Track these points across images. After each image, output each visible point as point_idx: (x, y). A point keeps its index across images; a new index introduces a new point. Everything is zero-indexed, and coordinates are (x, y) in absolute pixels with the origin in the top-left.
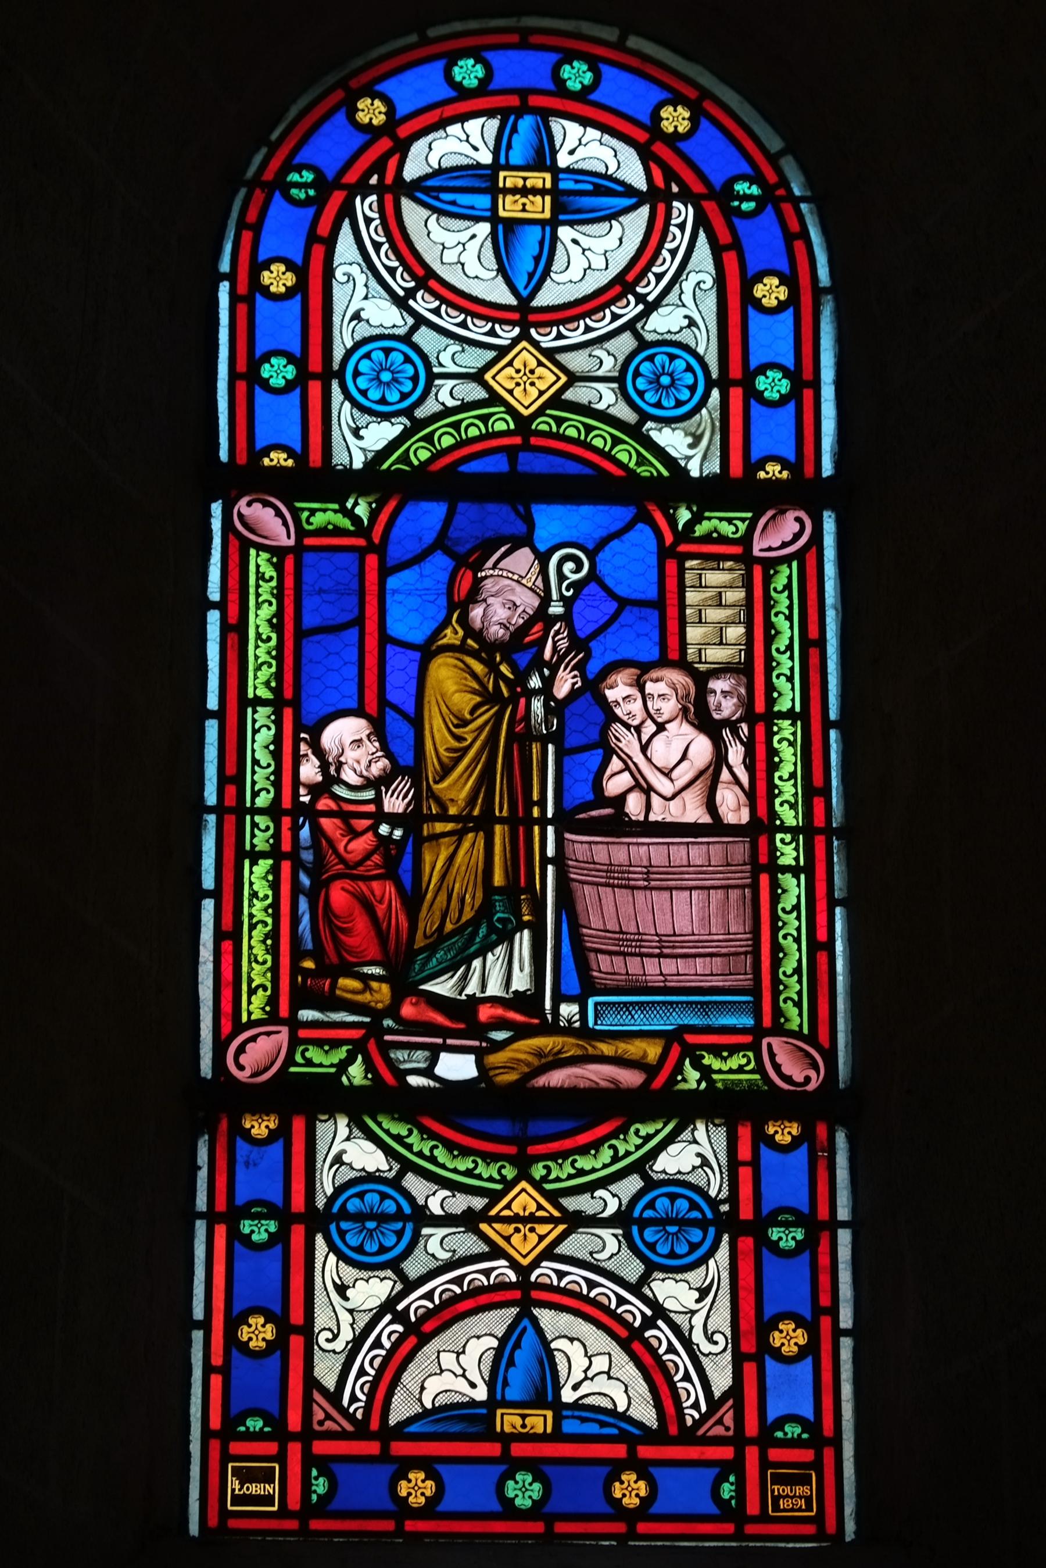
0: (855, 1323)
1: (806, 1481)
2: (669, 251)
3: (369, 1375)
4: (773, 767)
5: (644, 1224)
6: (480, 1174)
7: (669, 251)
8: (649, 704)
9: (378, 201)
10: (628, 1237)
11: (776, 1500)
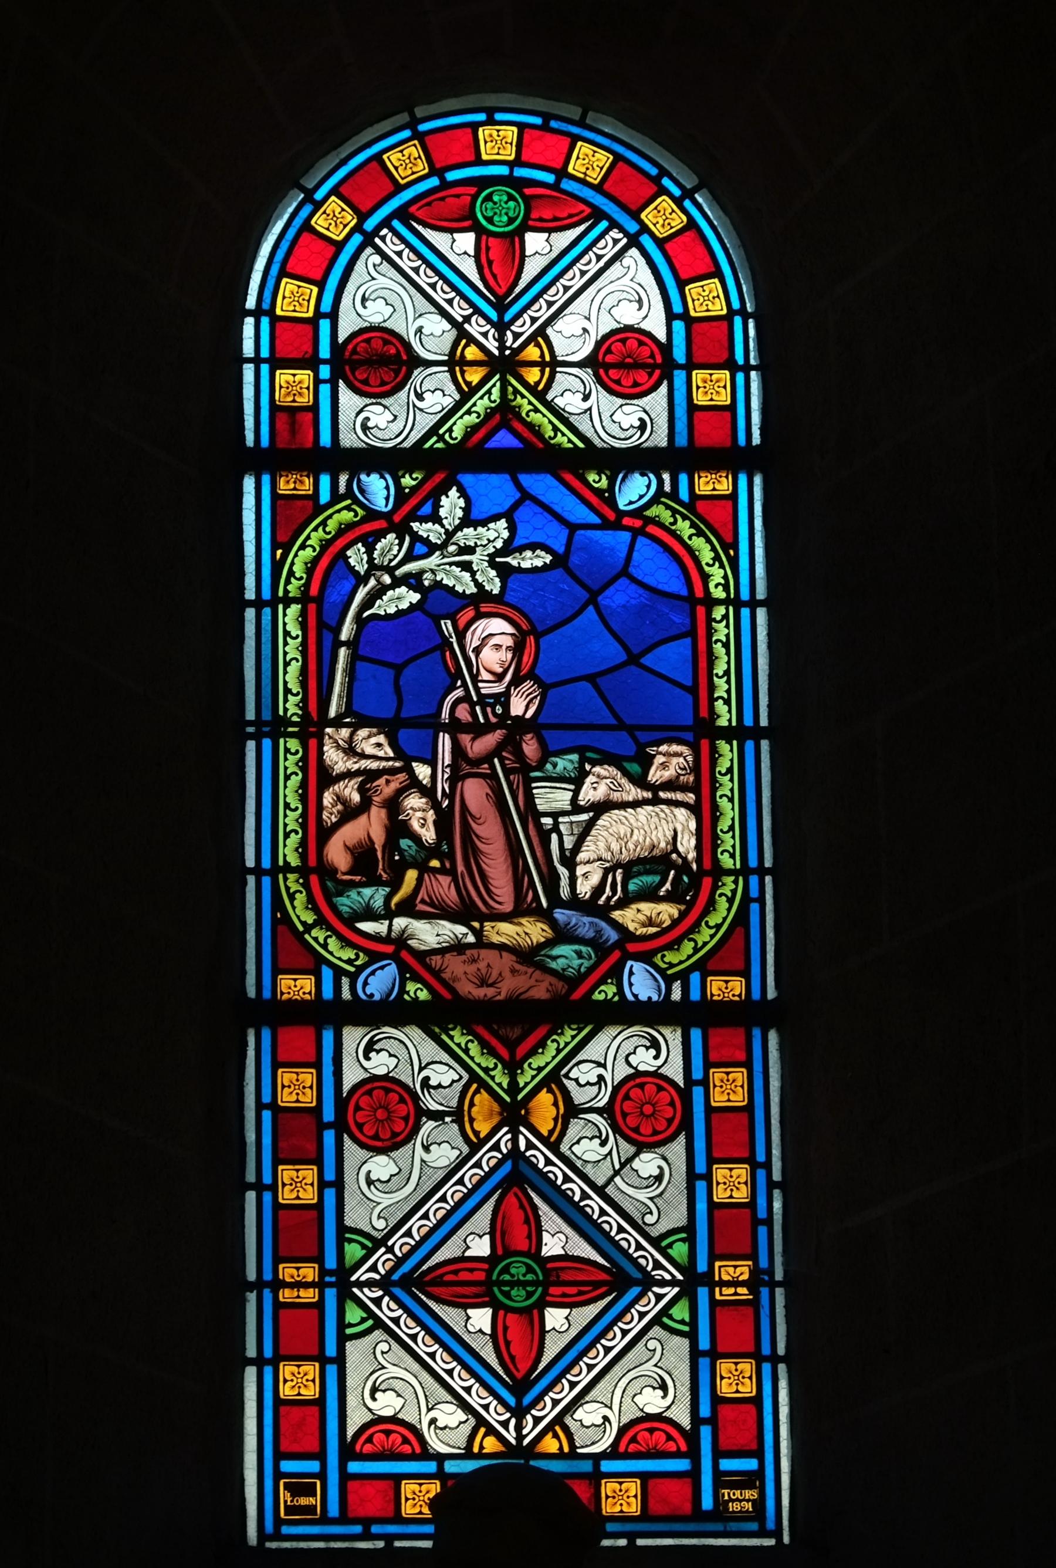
0: (769, 723)
4: (715, 820)
5: (607, 367)
6: (480, 1092)
9: (391, 1299)
10: (596, 375)
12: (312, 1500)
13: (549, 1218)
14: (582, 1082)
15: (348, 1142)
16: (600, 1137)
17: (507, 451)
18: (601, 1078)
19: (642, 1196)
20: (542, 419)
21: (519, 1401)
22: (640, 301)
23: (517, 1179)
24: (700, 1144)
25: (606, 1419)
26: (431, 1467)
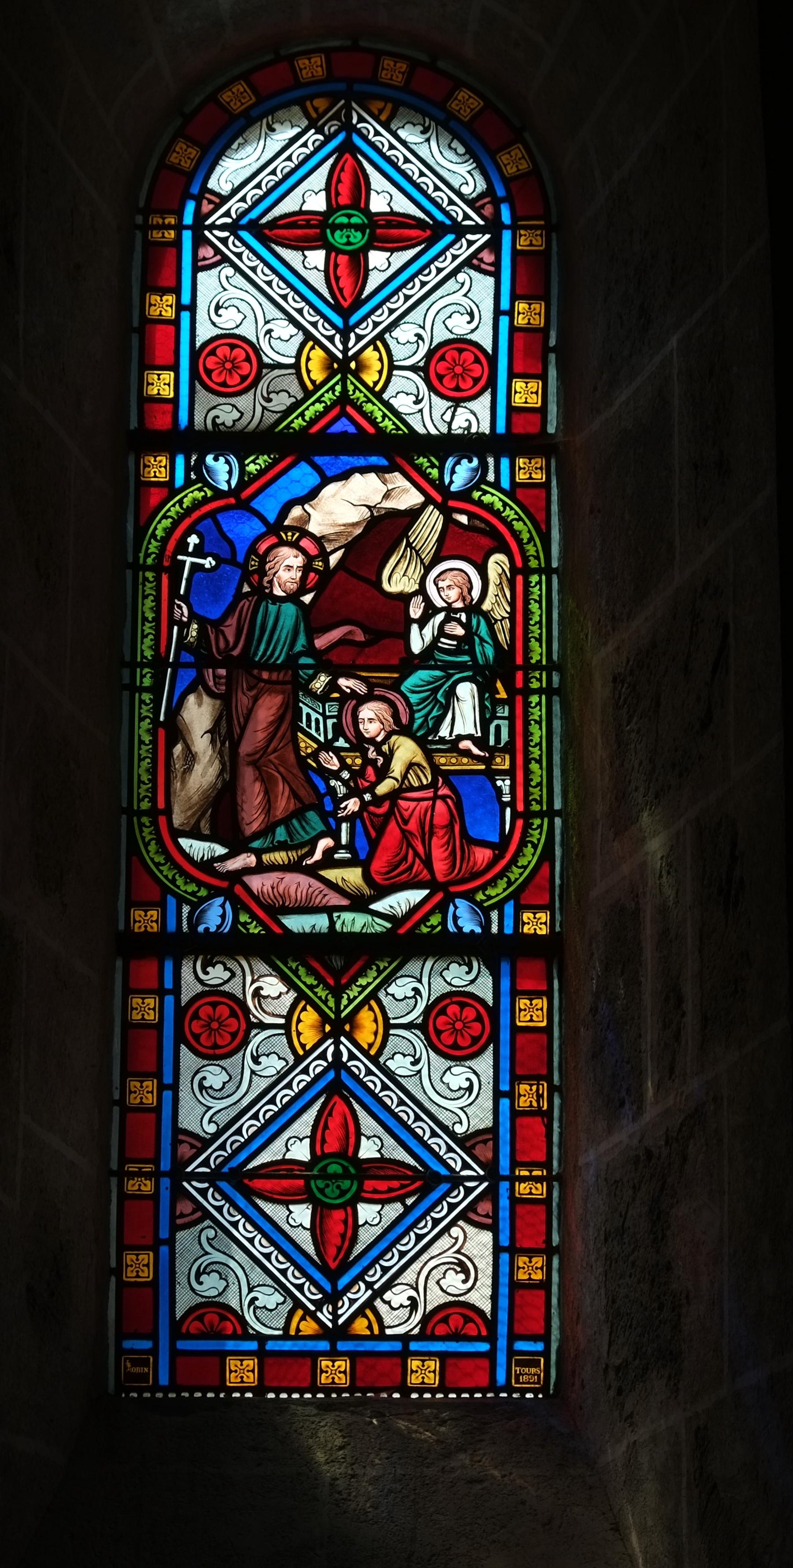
1: (537, 1364)
2: (374, 322)
3: (226, 1151)
7: (374, 322)
8: (442, 594)
11: (517, 1377)
12: (146, 1370)
13: (367, 1123)
14: (395, 1304)
15: (183, 1049)
16: (414, 1057)
17: (335, 964)
18: (417, 991)
19: (452, 1105)
20: (376, 410)
21: (338, 1075)
22: (471, 314)
23: (337, 1087)
24: (505, 1065)
25: (417, 991)
26: (253, 1346)
